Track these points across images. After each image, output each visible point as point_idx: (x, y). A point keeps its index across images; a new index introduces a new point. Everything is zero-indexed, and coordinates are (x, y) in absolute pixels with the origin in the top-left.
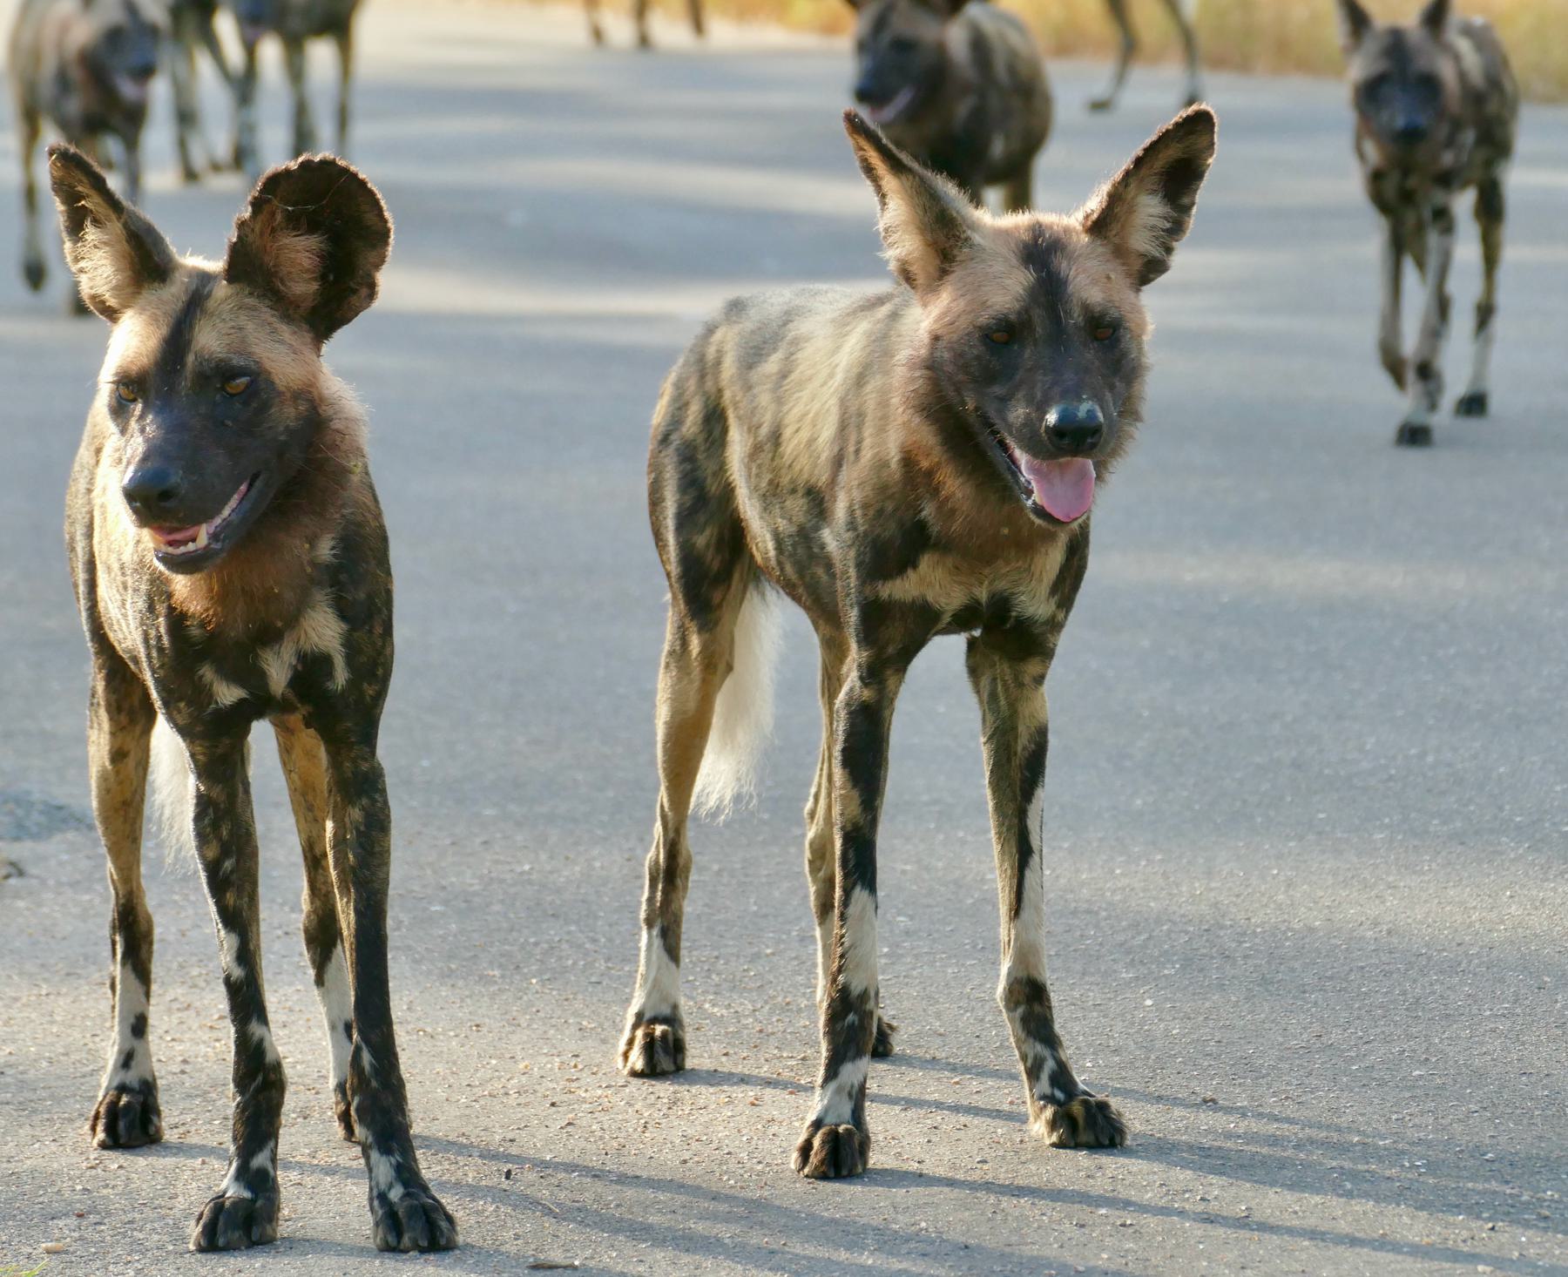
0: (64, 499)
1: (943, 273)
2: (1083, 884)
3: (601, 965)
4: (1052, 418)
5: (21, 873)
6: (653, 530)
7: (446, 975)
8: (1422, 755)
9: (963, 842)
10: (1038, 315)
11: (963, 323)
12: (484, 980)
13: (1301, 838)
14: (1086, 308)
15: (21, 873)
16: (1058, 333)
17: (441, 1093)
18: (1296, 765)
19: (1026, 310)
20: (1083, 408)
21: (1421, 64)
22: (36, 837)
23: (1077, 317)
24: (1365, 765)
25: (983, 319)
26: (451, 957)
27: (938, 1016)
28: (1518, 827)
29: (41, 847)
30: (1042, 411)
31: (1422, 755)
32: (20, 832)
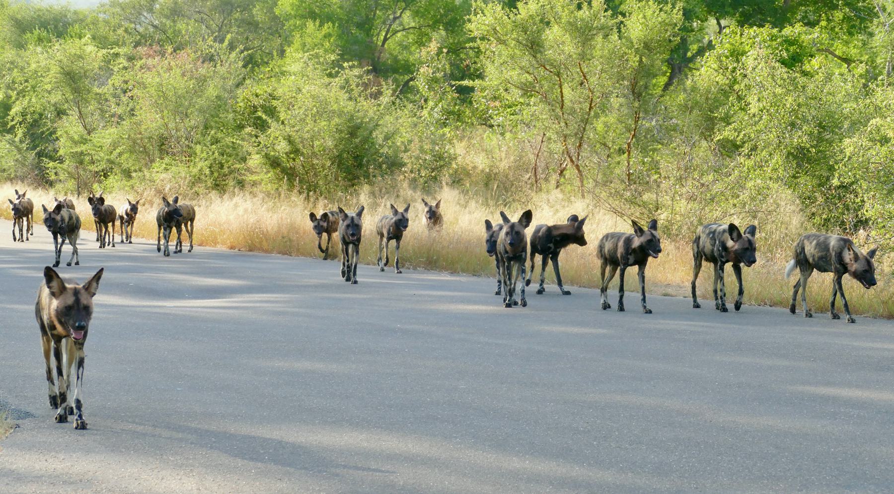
0: (874, 277)
1: (60, 295)
2: (253, 432)
3: (147, 448)
4: (77, 324)
5: (19, 427)
6: (85, 340)
7: (112, 451)
8: (327, 404)
9: (226, 422)
10: (75, 305)
11: (63, 305)
12: (121, 452)
13: (300, 422)
14: (83, 304)
15: (19, 427)
16: (79, 309)
17: (111, 476)
18: (299, 406)
19: (73, 304)
20: (82, 323)
21: (356, 222)
22: (22, 419)
23: (82, 306)
24: (314, 406)
25: (66, 305)
26: (114, 446)
27: (221, 460)
28: (347, 420)
29: (24, 421)
30: (75, 323)
31: (327, 404)
32: (19, 418)
